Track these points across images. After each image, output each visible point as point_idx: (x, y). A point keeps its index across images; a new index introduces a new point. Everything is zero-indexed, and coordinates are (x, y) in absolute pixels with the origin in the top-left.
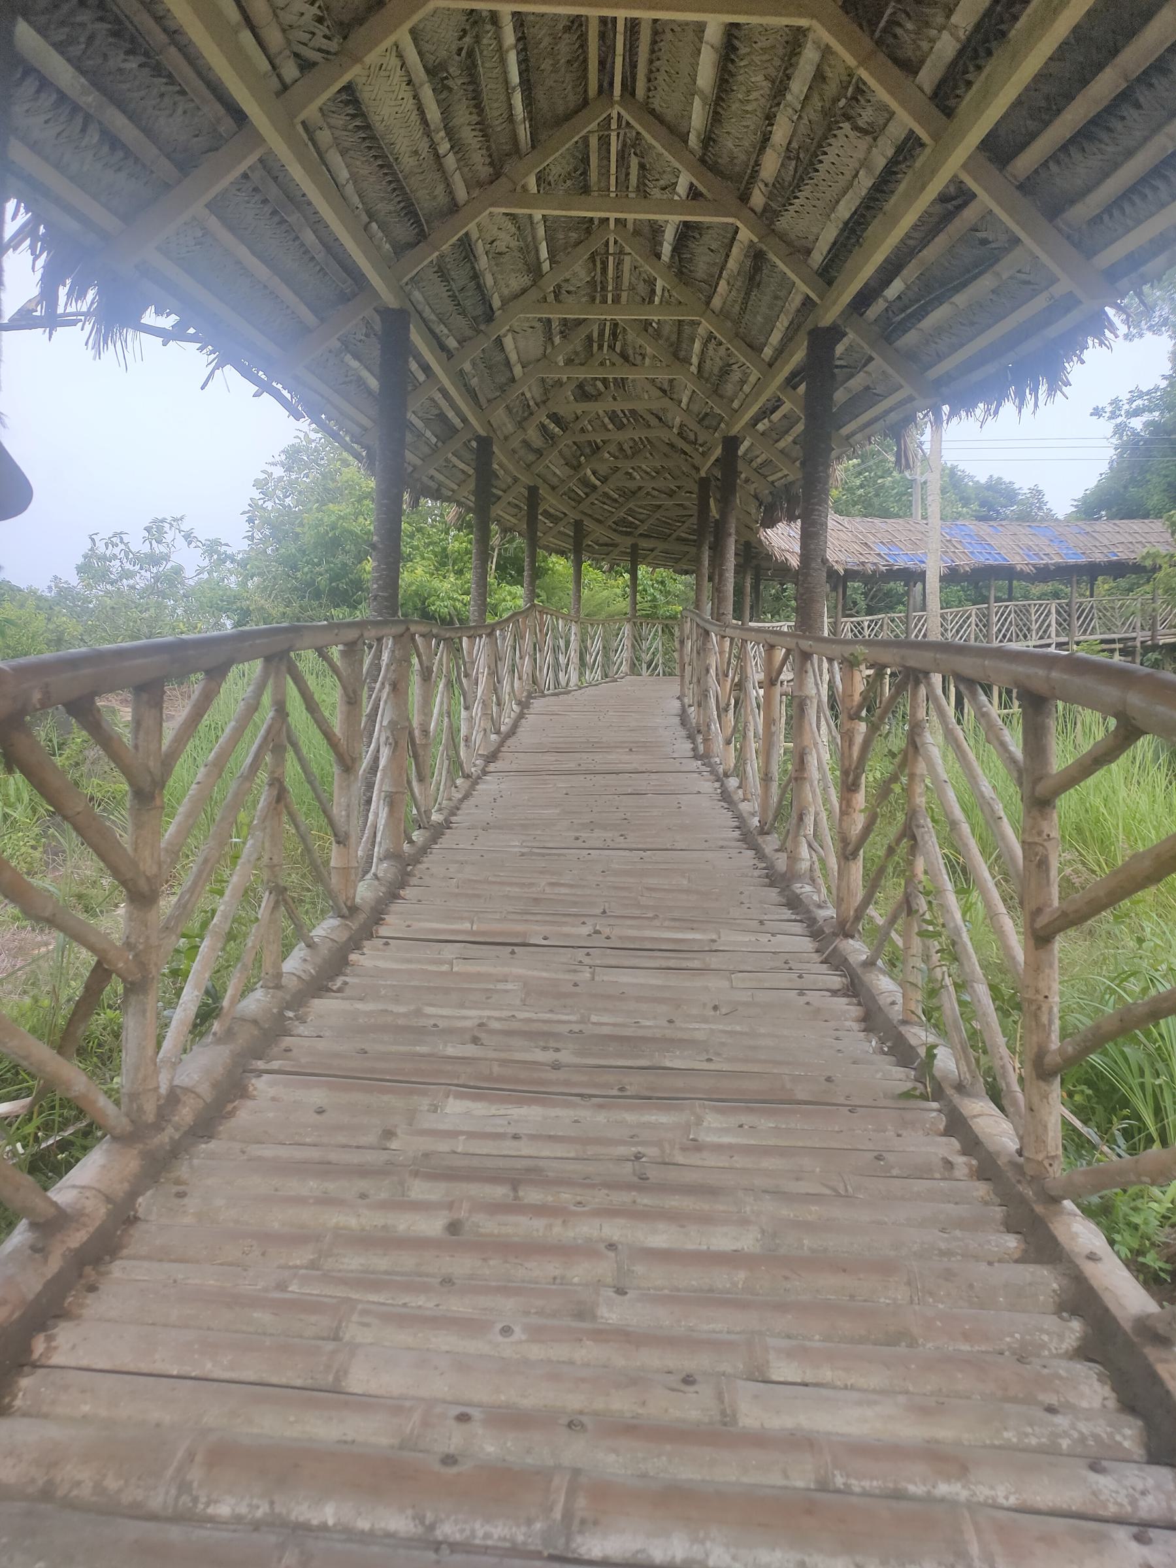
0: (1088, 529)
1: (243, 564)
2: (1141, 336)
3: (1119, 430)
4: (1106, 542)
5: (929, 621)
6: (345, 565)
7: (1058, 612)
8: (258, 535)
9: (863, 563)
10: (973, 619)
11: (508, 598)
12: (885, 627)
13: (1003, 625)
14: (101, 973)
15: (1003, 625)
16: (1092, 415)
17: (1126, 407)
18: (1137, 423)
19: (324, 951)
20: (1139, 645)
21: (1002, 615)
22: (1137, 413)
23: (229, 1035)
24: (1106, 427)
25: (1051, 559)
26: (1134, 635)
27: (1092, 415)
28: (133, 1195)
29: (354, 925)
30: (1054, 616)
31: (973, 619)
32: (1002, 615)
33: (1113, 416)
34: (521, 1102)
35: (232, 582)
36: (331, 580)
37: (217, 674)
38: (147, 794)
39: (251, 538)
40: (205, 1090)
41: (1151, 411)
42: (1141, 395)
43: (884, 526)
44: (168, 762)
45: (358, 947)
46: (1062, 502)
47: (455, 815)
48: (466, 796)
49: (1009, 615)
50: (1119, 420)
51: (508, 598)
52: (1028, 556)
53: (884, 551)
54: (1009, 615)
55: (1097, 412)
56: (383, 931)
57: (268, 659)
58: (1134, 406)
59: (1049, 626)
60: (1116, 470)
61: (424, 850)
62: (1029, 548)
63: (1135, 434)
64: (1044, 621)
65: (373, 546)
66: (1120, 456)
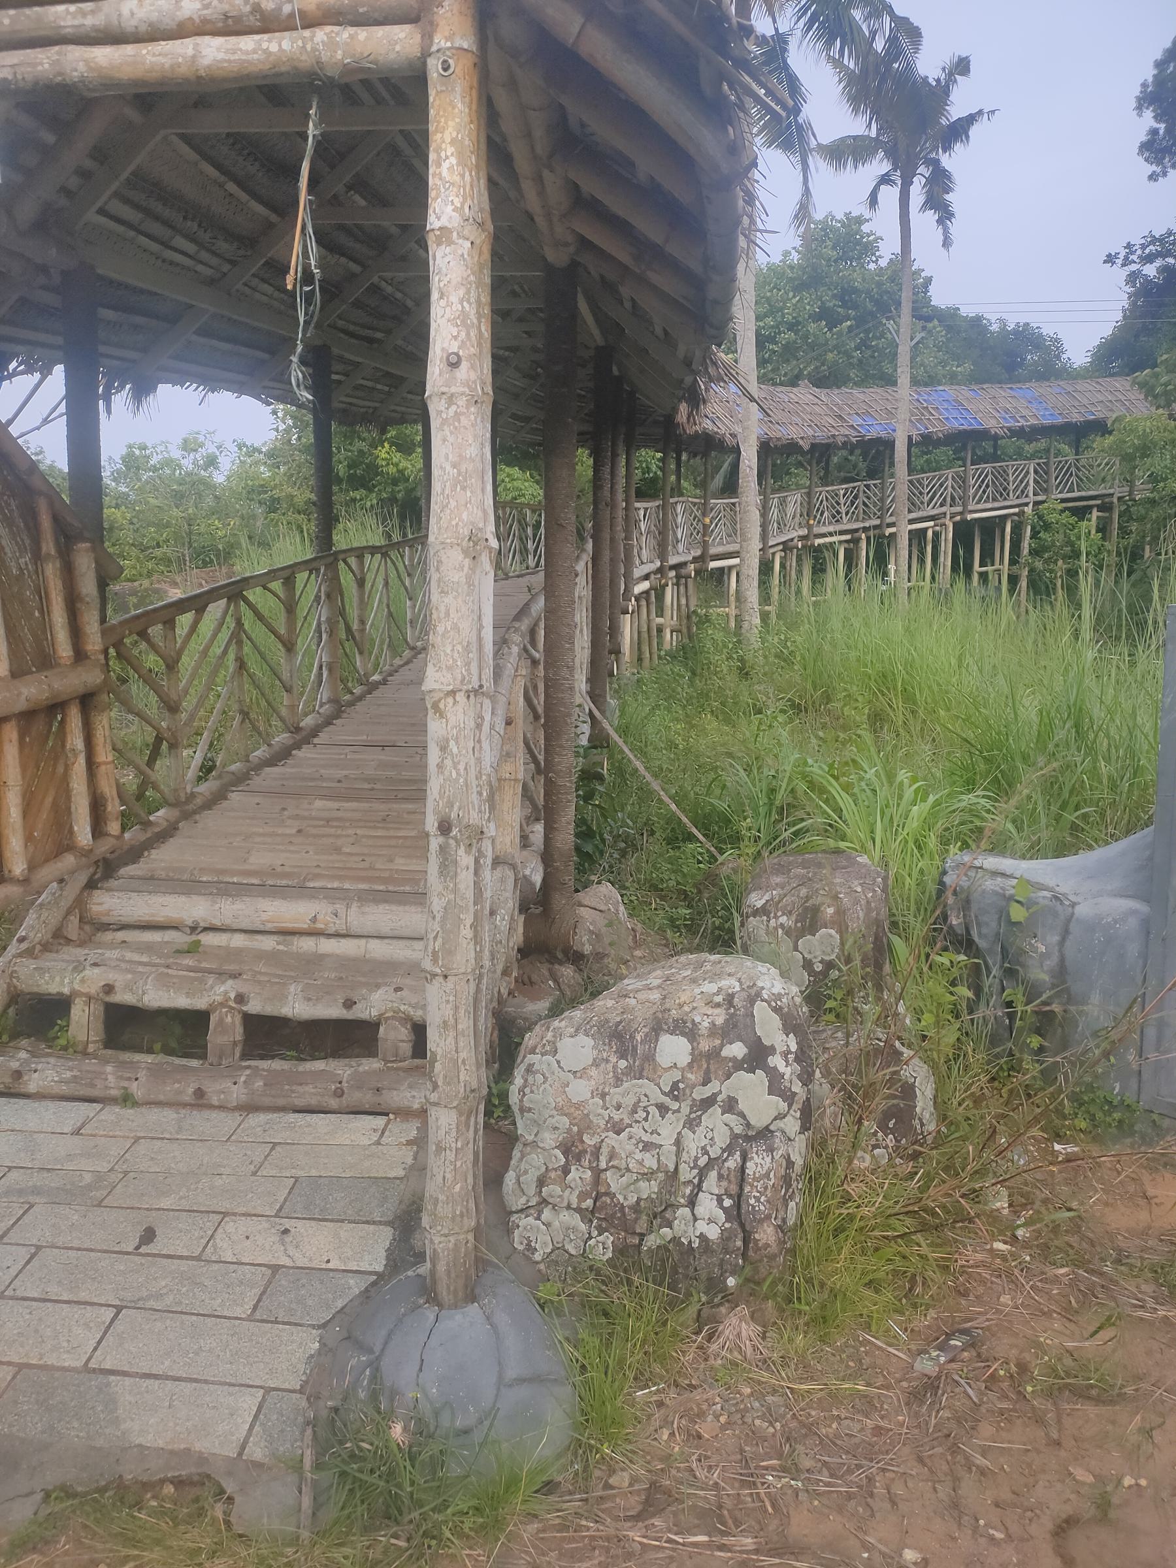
0: (1070, 389)
1: (271, 454)
2: (1165, 174)
3: (1132, 278)
4: (1085, 402)
5: (897, 488)
6: (361, 451)
7: (1036, 472)
8: (282, 427)
9: (833, 436)
10: (950, 482)
11: (507, 480)
12: (861, 494)
13: (980, 487)
14: (159, 740)
15: (980, 487)
16: (1105, 262)
17: (1139, 252)
18: (1150, 270)
19: (276, 748)
20: (1115, 500)
21: (980, 476)
22: (1148, 259)
23: (220, 777)
24: (1119, 274)
25: (1027, 421)
26: (1111, 491)
27: (1105, 262)
28: (177, 822)
29: (298, 737)
30: (1032, 475)
31: (950, 482)
32: (980, 476)
33: (1126, 262)
34: (348, 801)
35: (265, 472)
36: (350, 467)
37: (201, 611)
38: (171, 666)
39: (277, 430)
40: (207, 794)
41: (1164, 257)
42: (1154, 240)
43: (861, 396)
44: (179, 653)
45: (299, 748)
46: (1078, 350)
47: (391, 675)
48: (406, 663)
49: (986, 476)
50: (1134, 267)
51: (507, 480)
52: (1005, 418)
53: (857, 421)
54: (986, 476)
55: (1110, 259)
56: (316, 740)
57: (229, 599)
58: (1147, 251)
59: (1025, 487)
60: (1130, 314)
61: (360, 698)
62: (1007, 411)
63: (1147, 281)
64: (1021, 482)
65: (314, 504)
66: (1134, 304)
